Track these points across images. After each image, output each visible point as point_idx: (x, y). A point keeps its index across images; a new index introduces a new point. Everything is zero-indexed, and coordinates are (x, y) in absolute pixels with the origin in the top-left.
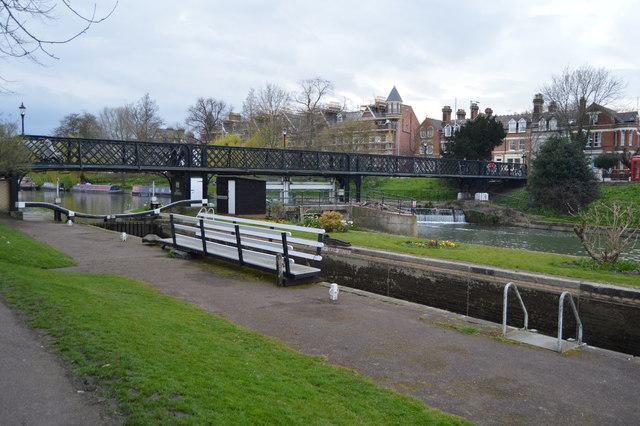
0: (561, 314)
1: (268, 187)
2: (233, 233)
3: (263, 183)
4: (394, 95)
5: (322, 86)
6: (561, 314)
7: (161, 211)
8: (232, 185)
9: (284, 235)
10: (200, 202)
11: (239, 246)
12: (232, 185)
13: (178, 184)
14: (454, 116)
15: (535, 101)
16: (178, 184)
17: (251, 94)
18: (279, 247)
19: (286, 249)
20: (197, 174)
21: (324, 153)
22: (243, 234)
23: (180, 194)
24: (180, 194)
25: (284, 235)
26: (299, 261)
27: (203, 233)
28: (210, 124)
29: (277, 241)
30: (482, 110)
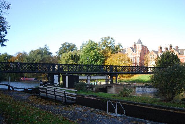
0: (107, 107)
1: (80, 78)
2: (53, 91)
3: (78, 77)
5: (110, 40)
6: (107, 107)
7: (43, 86)
8: (67, 77)
9: (65, 92)
10: (57, 83)
11: (55, 95)
12: (67, 77)
13: (50, 77)
14: (163, 49)
16: (50, 77)
17: (52, 53)
18: (63, 95)
19: (65, 95)
20: (56, 74)
21: (84, 65)
22: (48, 90)
23: (50, 81)
24: (50, 81)
25: (65, 92)
26: (69, 98)
27: (55, 93)
28: (105, 45)
29: (63, 93)
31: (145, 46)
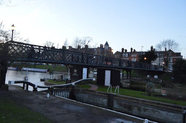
1: (97, 73)
4: (107, 44)
5: (89, 39)
13: (75, 71)
15: (151, 48)
30: (83, 46)
31: (111, 48)
